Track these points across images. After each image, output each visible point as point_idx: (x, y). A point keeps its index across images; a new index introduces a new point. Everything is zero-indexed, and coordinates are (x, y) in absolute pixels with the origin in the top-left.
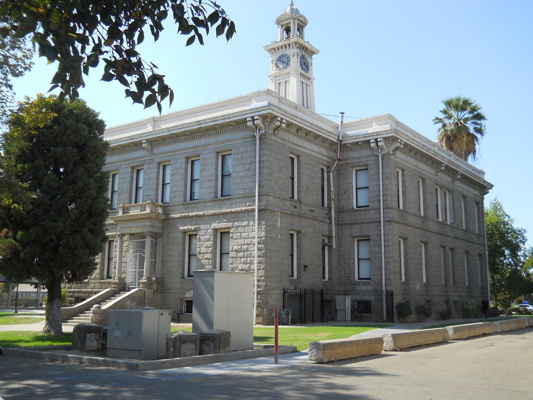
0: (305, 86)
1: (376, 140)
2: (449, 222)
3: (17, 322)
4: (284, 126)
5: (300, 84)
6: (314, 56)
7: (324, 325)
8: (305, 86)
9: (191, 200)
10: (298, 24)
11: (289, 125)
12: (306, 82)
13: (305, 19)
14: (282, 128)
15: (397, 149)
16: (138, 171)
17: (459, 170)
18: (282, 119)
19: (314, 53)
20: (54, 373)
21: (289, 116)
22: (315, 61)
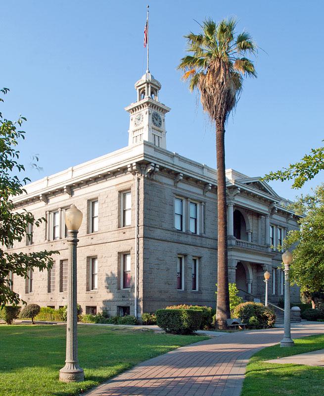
0: (156, 137)
1: (131, 164)
2: (198, 233)
3: (261, 331)
4: (157, 170)
5: (152, 137)
6: (167, 114)
7: (314, 333)
8: (156, 137)
9: (124, 226)
10: (151, 87)
11: (161, 168)
12: (158, 134)
13: (161, 86)
14: (156, 172)
15: (152, 172)
16: (93, 203)
17: (291, 213)
18: (155, 164)
19: (166, 111)
20: (172, 347)
21: (171, 165)
22: (168, 119)
